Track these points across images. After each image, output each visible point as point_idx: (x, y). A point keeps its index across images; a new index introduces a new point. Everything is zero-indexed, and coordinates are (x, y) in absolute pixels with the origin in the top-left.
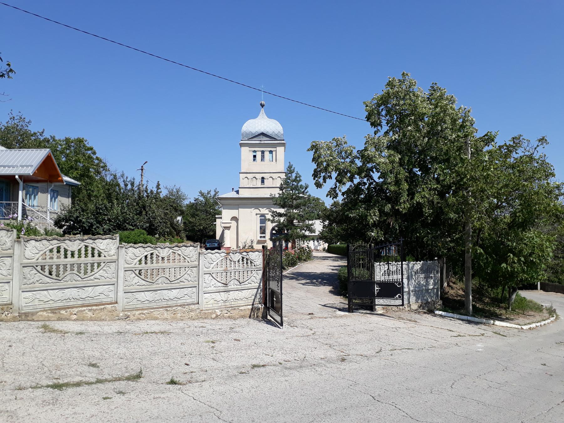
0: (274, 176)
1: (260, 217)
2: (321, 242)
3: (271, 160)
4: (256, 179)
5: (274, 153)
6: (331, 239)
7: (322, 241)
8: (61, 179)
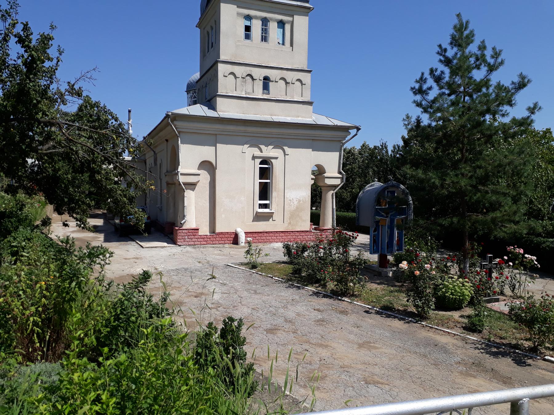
0: (290, 76)
1: (261, 163)
3: (281, 42)
4: (253, 79)
5: (288, 27)
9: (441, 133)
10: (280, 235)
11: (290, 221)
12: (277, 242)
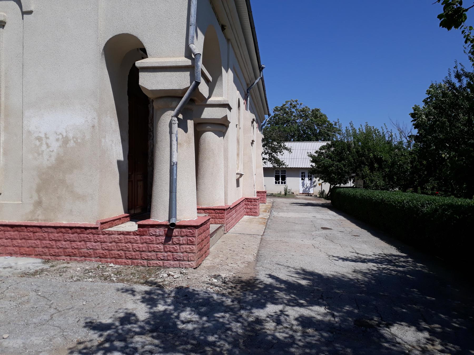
2: (316, 180)
6: (339, 174)
7: (318, 179)
8: (286, 285)
9: (109, 112)
10: (51, 236)
11: (40, 197)
12: (11, 254)
